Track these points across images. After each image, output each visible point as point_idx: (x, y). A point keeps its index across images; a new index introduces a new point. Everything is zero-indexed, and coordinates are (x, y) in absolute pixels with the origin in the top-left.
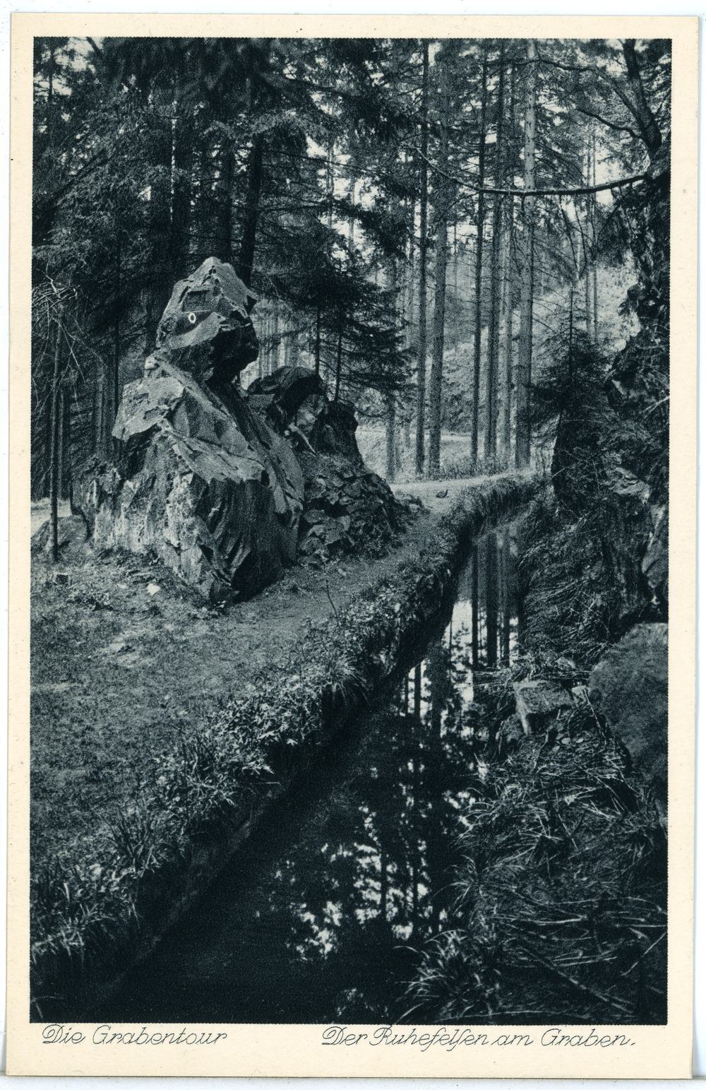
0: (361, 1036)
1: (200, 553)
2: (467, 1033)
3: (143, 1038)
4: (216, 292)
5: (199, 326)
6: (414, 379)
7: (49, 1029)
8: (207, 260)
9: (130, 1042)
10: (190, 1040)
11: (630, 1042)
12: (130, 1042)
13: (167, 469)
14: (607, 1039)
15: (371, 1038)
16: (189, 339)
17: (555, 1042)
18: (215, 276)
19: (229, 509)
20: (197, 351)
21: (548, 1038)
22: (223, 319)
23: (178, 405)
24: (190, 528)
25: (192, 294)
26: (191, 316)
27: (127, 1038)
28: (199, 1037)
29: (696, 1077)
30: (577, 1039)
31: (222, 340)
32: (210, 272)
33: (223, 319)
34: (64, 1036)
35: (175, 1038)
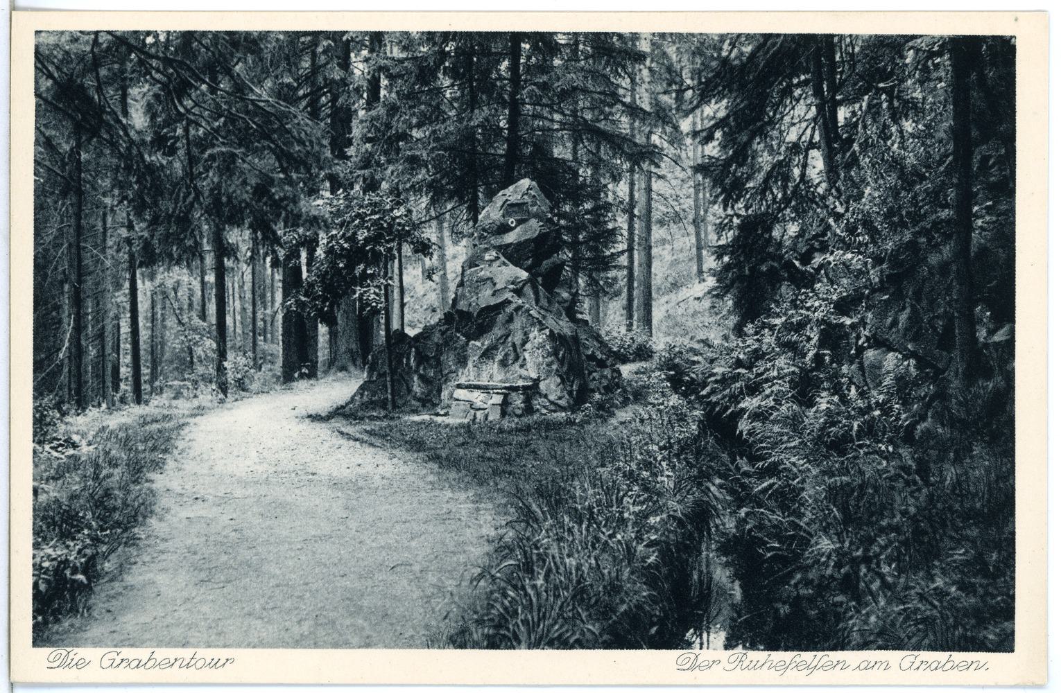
0: (714, 662)
1: (559, 380)
2: (825, 659)
3: (949, 666)
4: (534, 204)
5: (518, 229)
6: (623, 260)
7: (54, 654)
8: (522, 181)
9: (936, 669)
10: (198, 665)
11: (986, 667)
12: (936, 669)
13: (523, 328)
14: (167, 661)
15: (724, 663)
16: (510, 238)
17: (913, 668)
18: (532, 193)
19: (333, 335)
20: (520, 246)
21: (906, 664)
22: (541, 224)
23: (524, 285)
24: (549, 365)
25: (512, 205)
26: (511, 221)
27: (134, 664)
28: (208, 661)
29: (12, 685)
30: (137, 662)
31: (540, 240)
32: (528, 189)
33: (541, 224)
34: (69, 661)
35: (185, 663)
